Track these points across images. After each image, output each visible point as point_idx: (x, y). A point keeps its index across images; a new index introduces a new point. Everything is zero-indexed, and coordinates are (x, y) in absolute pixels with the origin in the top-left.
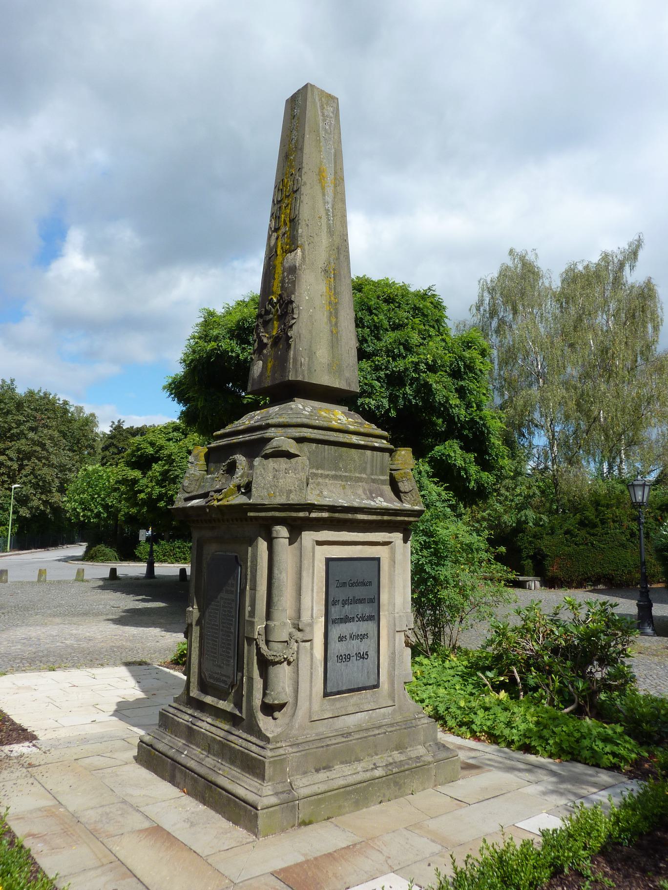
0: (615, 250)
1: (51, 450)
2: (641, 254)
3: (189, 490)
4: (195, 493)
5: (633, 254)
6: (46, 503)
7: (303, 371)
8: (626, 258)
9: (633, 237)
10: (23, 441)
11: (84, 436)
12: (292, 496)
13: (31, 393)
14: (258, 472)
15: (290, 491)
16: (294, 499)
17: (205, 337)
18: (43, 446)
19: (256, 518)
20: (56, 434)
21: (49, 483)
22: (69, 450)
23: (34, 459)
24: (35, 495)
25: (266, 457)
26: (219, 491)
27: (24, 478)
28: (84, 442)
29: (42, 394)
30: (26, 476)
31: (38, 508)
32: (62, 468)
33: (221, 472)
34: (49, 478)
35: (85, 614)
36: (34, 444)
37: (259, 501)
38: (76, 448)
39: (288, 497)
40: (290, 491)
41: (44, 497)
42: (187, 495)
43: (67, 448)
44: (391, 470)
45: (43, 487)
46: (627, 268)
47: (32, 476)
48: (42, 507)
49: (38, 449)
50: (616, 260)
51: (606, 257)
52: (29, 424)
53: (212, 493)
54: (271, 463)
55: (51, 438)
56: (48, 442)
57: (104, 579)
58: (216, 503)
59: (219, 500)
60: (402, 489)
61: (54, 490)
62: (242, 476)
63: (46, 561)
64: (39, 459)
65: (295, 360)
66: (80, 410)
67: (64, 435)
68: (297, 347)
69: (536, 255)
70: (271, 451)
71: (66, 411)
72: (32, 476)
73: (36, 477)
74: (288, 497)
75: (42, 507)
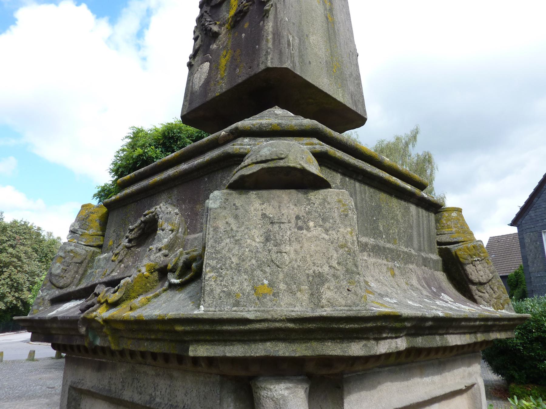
0: (403, 135)
1: (25, 261)
2: (418, 137)
3: (62, 283)
4: (73, 288)
5: (414, 137)
6: (18, 299)
7: (292, 56)
8: (410, 139)
9: (413, 127)
10: (4, 254)
11: (51, 251)
12: (328, 293)
13: (15, 222)
14: (221, 224)
15: (318, 280)
16: (335, 302)
17: (133, 146)
18: (19, 259)
19: (211, 361)
20: (30, 250)
21: (21, 285)
22: (39, 261)
23: (11, 267)
24: (10, 293)
25: (243, 185)
26: (113, 283)
27: (3, 281)
28: (50, 255)
29: (23, 223)
30: (4, 279)
31: (11, 303)
32: (32, 274)
33: (125, 242)
34: (21, 281)
35: (19, 397)
36: (13, 257)
37: (228, 311)
38: (44, 260)
39: (315, 297)
40: (318, 280)
41: (16, 295)
42: (57, 293)
43: (37, 260)
44: (439, 244)
45: (16, 287)
46: (410, 146)
47: (9, 280)
48: (15, 302)
49: (15, 260)
50: (403, 141)
51: (398, 139)
52: (9, 243)
53: (101, 290)
54: (255, 204)
55: (26, 253)
56: (23, 255)
57: (52, 358)
58: (102, 313)
59: (115, 304)
60: (474, 277)
61: (25, 289)
62: (171, 247)
63: (13, 343)
64: (16, 267)
65: (277, 35)
66: (50, 234)
67: (36, 251)
68: (281, 15)
69: (357, 135)
70: (256, 168)
71: (39, 235)
72: (9, 280)
73: (12, 280)
74: (315, 297)
75: (15, 302)
